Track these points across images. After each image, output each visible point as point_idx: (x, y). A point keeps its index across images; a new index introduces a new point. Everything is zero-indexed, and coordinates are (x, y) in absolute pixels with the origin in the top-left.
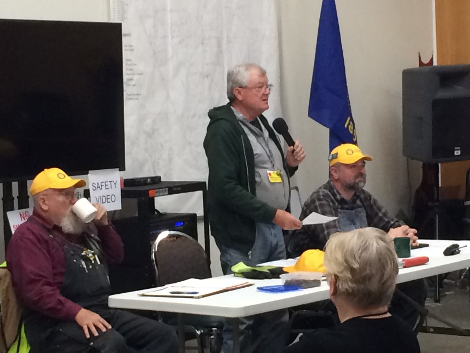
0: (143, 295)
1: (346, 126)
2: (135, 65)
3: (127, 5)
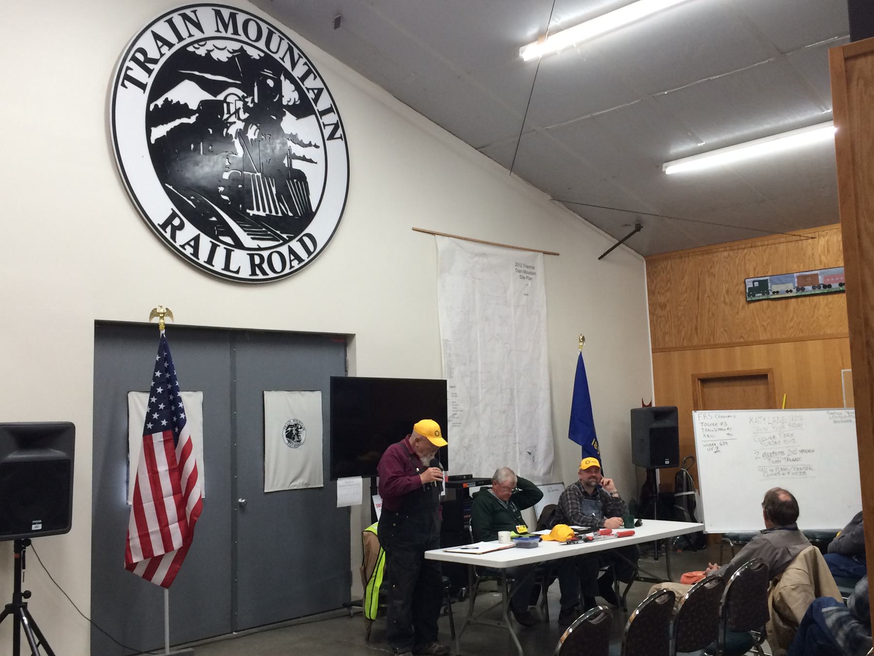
0: (446, 552)
1: (592, 444)
2: (458, 405)
3: (453, 369)
